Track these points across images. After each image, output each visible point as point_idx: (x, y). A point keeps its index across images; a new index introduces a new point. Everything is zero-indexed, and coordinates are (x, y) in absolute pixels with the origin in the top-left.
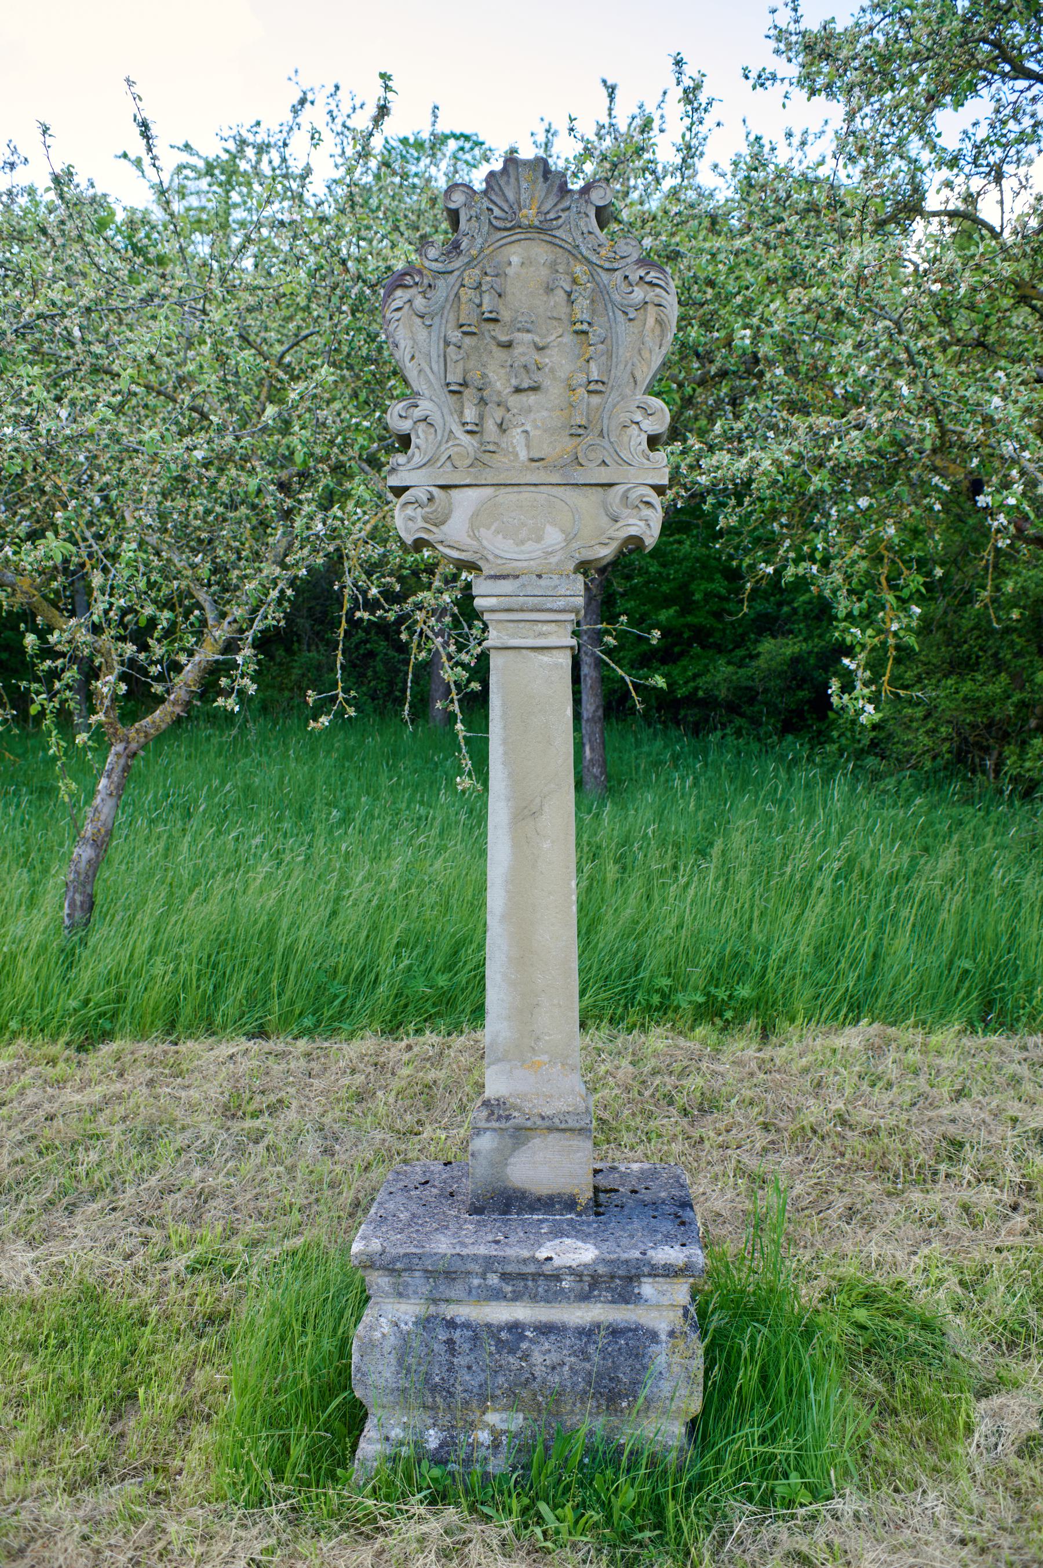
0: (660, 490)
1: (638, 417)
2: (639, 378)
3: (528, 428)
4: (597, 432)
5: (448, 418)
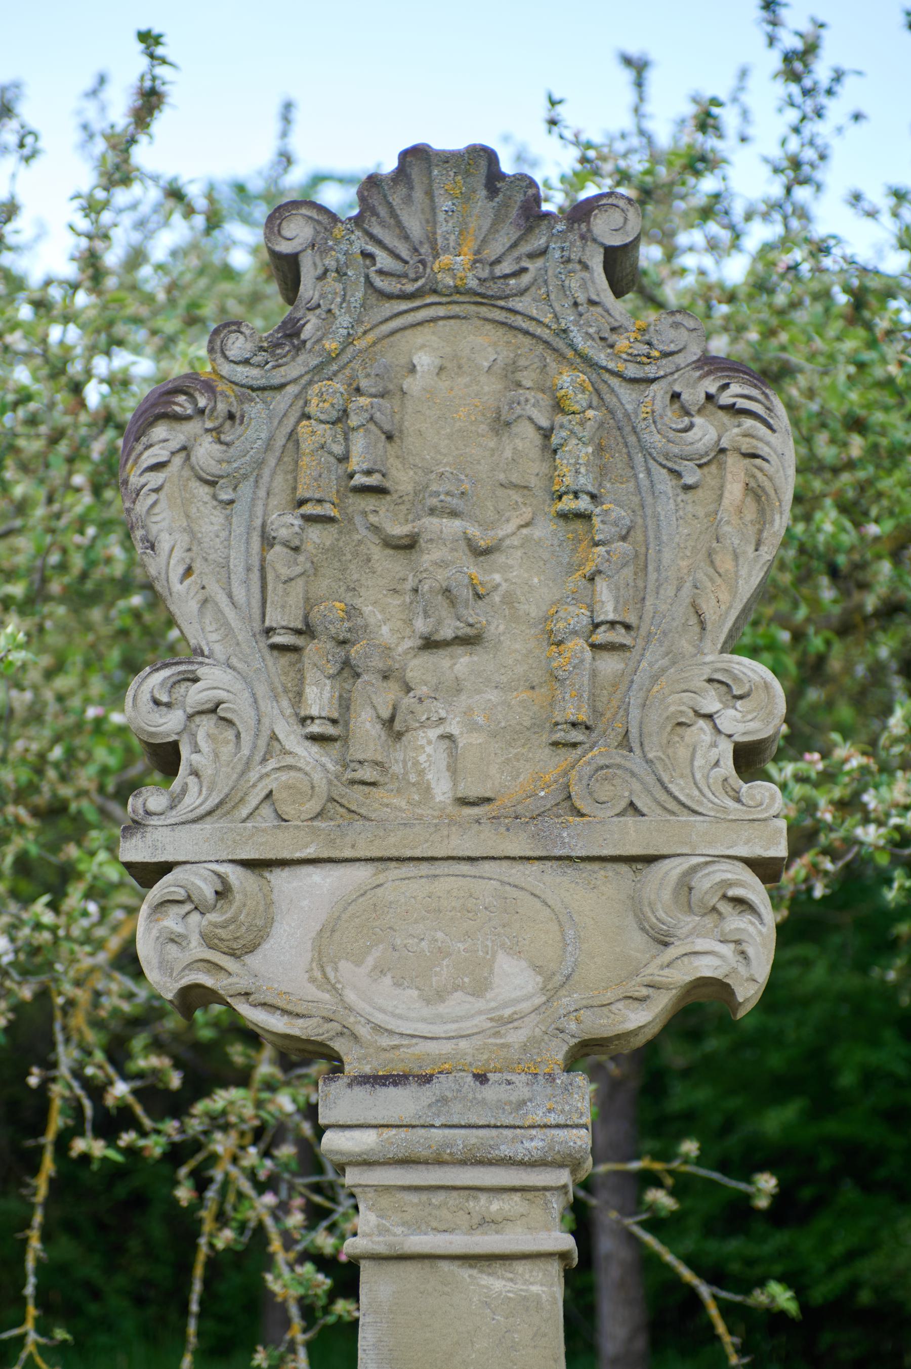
0: (767, 870)
1: (711, 703)
2: (710, 612)
3: (454, 728)
4: (614, 738)
5: (267, 706)
